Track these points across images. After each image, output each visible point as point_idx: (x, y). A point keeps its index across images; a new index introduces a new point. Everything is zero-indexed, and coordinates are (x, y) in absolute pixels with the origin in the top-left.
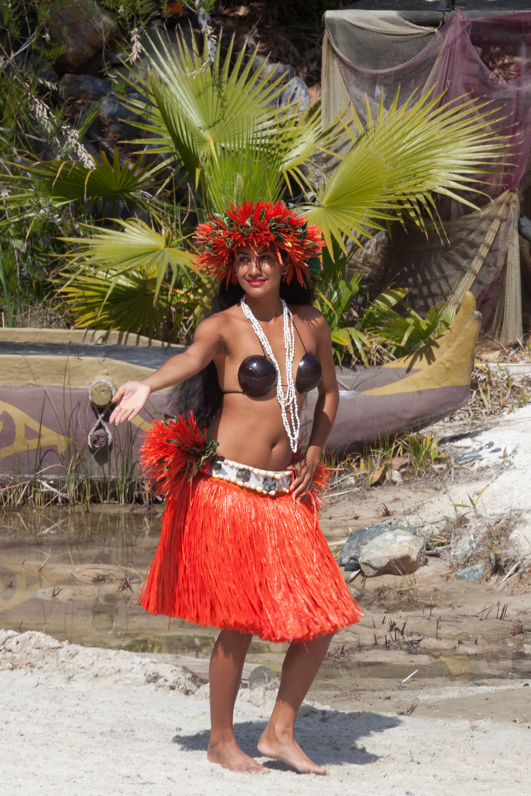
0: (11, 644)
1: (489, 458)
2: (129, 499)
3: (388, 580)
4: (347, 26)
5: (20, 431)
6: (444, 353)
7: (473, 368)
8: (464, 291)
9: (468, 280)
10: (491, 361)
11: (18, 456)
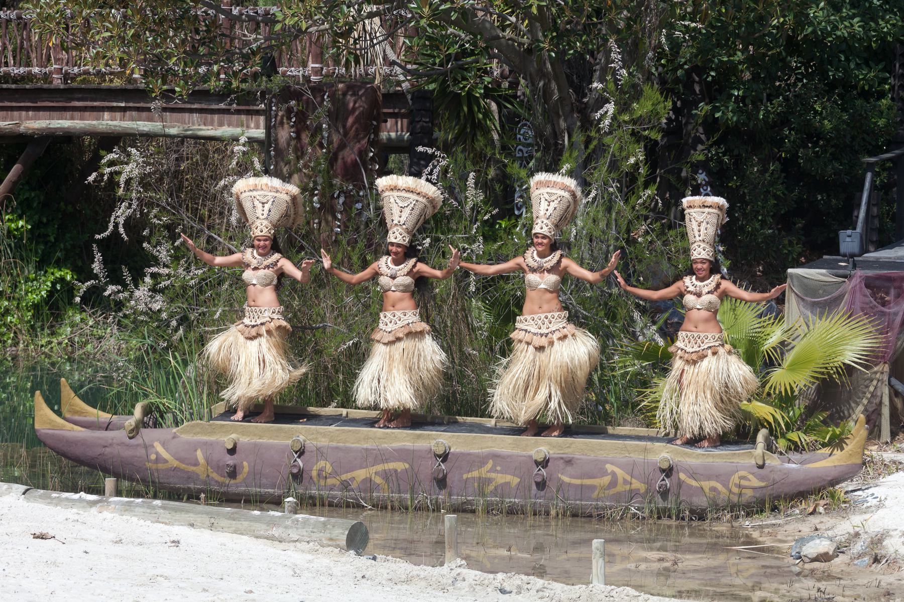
0: (613, 593)
1: (872, 502)
2: (678, 518)
3: (816, 565)
4: (799, 277)
5: (620, 480)
6: (851, 446)
7: (864, 454)
8: (859, 414)
9: (861, 408)
10: (873, 451)
11: (619, 493)
